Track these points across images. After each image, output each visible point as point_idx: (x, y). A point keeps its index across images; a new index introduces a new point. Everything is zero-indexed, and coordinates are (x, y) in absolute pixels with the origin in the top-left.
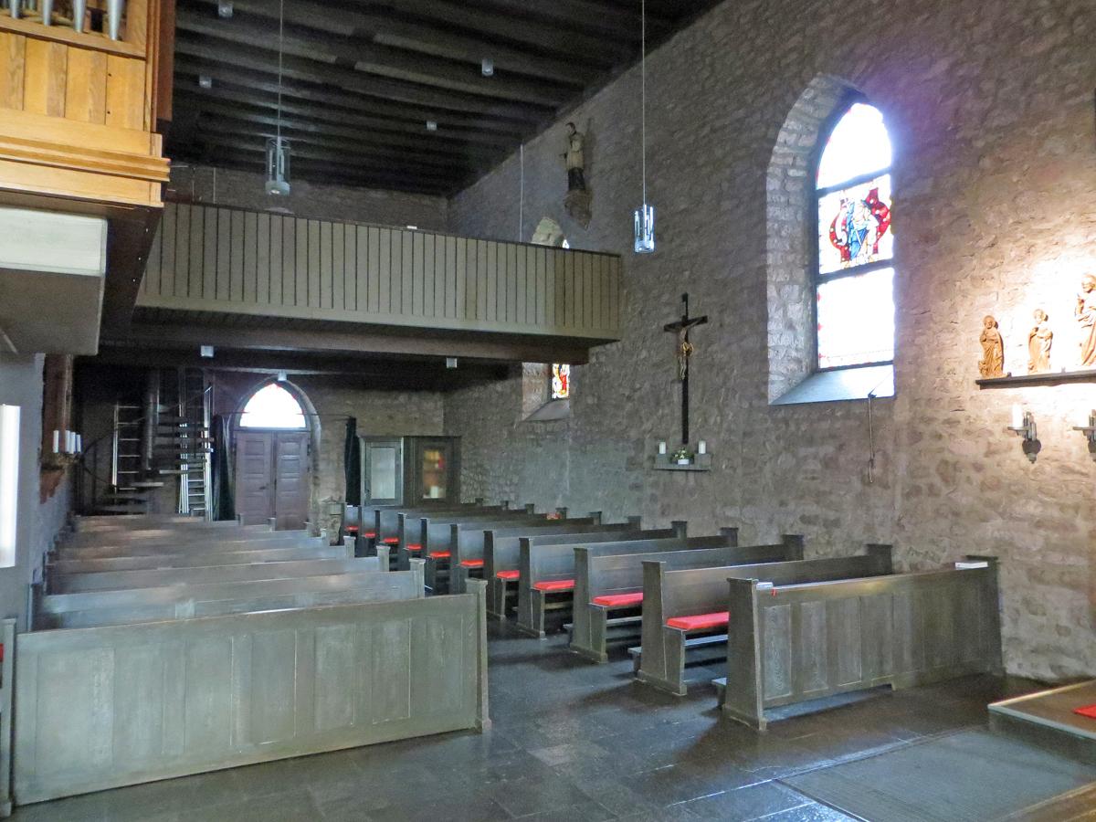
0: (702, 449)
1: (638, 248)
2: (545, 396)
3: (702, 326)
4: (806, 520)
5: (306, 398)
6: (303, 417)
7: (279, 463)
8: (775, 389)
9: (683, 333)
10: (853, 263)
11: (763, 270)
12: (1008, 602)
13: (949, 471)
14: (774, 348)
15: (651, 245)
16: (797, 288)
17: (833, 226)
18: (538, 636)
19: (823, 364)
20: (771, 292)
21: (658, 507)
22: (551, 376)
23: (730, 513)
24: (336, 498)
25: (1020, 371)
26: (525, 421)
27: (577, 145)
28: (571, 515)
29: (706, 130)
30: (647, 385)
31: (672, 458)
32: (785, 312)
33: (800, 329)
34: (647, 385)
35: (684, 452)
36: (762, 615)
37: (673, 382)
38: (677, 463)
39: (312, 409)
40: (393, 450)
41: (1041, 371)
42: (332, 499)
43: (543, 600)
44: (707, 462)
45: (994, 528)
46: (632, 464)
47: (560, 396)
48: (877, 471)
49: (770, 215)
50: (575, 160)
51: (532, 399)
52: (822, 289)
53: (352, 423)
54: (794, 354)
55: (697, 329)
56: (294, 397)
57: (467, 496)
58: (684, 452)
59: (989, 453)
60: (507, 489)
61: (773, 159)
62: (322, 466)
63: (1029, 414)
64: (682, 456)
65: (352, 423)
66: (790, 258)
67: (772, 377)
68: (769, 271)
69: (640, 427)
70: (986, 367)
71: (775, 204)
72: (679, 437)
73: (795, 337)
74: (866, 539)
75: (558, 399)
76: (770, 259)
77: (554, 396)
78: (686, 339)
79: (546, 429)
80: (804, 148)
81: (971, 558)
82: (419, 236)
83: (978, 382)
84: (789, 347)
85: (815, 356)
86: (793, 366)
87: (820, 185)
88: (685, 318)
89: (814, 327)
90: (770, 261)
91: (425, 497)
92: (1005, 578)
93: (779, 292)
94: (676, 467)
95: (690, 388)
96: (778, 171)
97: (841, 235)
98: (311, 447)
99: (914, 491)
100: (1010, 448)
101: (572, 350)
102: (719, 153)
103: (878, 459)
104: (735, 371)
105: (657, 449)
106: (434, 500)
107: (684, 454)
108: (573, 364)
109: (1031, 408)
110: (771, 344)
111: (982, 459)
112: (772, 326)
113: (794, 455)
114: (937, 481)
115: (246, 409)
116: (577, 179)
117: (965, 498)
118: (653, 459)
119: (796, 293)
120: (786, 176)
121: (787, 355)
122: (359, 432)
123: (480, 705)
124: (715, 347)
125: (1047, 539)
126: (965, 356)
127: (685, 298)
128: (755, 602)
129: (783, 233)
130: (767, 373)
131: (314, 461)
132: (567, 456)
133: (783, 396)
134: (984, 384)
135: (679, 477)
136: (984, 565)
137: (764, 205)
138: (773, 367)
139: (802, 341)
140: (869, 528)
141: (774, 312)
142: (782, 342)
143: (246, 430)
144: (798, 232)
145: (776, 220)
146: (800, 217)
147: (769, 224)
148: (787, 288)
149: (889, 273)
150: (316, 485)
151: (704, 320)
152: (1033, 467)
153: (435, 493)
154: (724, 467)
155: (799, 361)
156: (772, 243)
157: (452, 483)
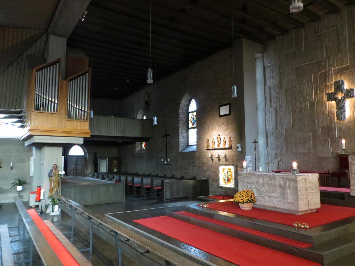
1: (154, 124)
2: (141, 148)
4: (185, 173)
5: (85, 148)
6: (83, 153)
7: (78, 164)
8: (180, 149)
9: (166, 137)
10: (194, 126)
11: (178, 127)
12: (210, 184)
13: (203, 164)
14: (180, 141)
15: (156, 124)
16: (185, 130)
17: (191, 119)
18: (135, 194)
19: (190, 144)
20: (180, 131)
22: (142, 144)
23: (174, 172)
24: (91, 172)
25: (211, 148)
26: (136, 154)
27: (147, 96)
28: (145, 174)
31: (164, 162)
32: (183, 135)
33: (185, 138)
36: (166, 186)
39: (86, 151)
40: (105, 160)
41: (213, 148)
42: (90, 172)
43: (136, 188)
45: (208, 173)
48: (194, 164)
49: (180, 117)
50: (146, 99)
51: (138, 149)
52: (189, 130)
53: (95, 154)
54: (184, 142)
56: (82, 148)
57: (123, 170)
59: (208, 161)
60: (132, 169)
61: (180, 106)
62: (88, 164)
63: (212, 155)
65: (95, 154)
66: (184, 124)
67: (180, 147)
68: (180, 127)
70: (207, 147)
71: (181, 115)
72: (165, 158)
73: (184, 140)
74: (192, 176)
76: (180, 125)
79: (141, 155)
80: (186, 104)
81: (205, 178)
82: (113, 118)
83: (206, 149)
84: (183, 141)
85: (188, 143)
86: (184, 145)
87: (190, 111)
88: (166, 134)
89: (188, 137)
90: (180, 125)
91: (113, 171)
92: (210, 180)
93: (181, 131)
96: (182, 108)
97: (192, 121)
98: (86, 160)
99: (199, 168)
100: (210, 160)
101: (146, 140)
103: (194, 162)
106: (115, 172)
108: (146, 142)
109: (213, 154)
110: (180, 141)
111: (207, 162)
112: (180, 137)
113: (183, 161)
114: (202, 165)
115: (70, 151)
116: (147, 103)
117: (205, 168)
119: (184, 132)
120: (183, 109)
121: (183, 143)
122: (97, 156)
123: (124, 198)
125: (214, 174)
126: (205, 145)
127: (166, 130)
128: (164, 183)
129: (182, 120)
130: (179, 146)
131: (86, 163)
133: (182, 150)
134: (208, 150)
136: (206, 179)
137: (179, 115)
138: (180, 145)
139: (186, 140)
140: (193, 174)
141: (181, 135)
142: (182, 140)
143: (70, 156)
144: (185, 120)
145: (181, 117)
146: (185, 117)
147: (180, 118)
148: (183, 130)
149: (196, 130)
150: (86, 169)
152: (213, 163)
153: (115, 170)
155: (185, 144)
156: (180, 122)
157: (119, 168)
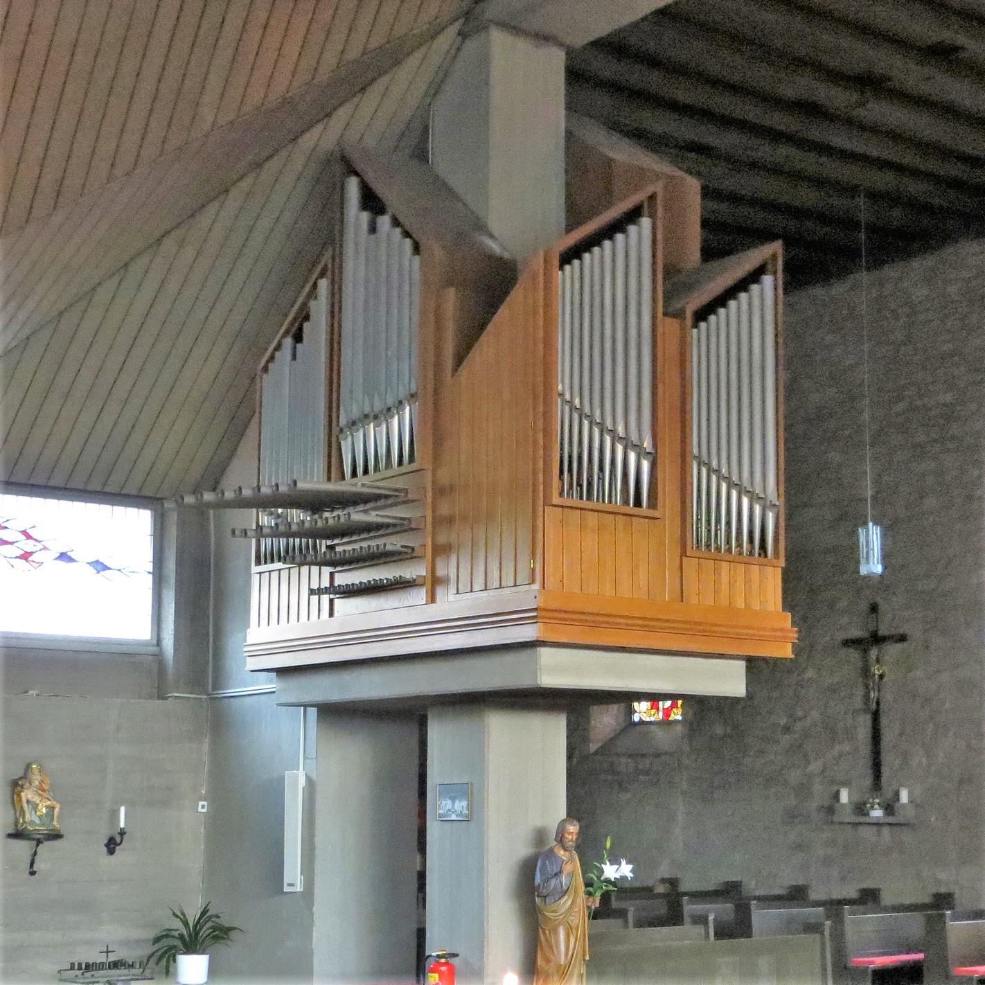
0: (904, 797)
2: (621, 719)
3: (899, 646)
15: (878, 569)
21: (835, 873)
29: (901, 406)
30: (815, 714)
31: (860, 808)
34: (815, 714)
35: (877, 801)
37: (856, 712)
38: (867, 814)
44: (911, 813)
46: (792, 816)
47: (647, 719)
55: (893, 650)
58: (877, 801)
64: (877, 806)
69: (806, 767)
72: (868, 781)
75: (642, 722)
77: (636, 718)
78: (878, 661)
94: (867, 820)
95: (884, 721)
102: (921, 438)
104: (947, 705)
105: (837, 796)
107: (879, 804)
118: (830, 810)
124: (919, 673)
127: (874, 608)
132: (680, 808)
135: (867, 833)
151: (902, 638)
154: (933, 819)
